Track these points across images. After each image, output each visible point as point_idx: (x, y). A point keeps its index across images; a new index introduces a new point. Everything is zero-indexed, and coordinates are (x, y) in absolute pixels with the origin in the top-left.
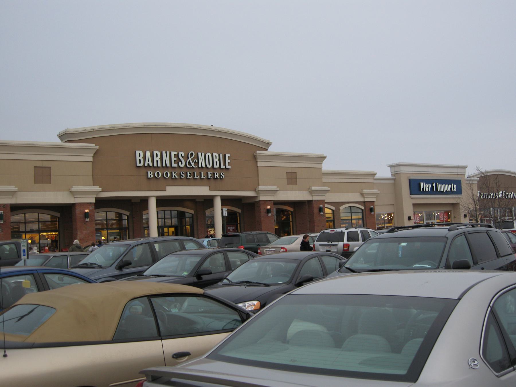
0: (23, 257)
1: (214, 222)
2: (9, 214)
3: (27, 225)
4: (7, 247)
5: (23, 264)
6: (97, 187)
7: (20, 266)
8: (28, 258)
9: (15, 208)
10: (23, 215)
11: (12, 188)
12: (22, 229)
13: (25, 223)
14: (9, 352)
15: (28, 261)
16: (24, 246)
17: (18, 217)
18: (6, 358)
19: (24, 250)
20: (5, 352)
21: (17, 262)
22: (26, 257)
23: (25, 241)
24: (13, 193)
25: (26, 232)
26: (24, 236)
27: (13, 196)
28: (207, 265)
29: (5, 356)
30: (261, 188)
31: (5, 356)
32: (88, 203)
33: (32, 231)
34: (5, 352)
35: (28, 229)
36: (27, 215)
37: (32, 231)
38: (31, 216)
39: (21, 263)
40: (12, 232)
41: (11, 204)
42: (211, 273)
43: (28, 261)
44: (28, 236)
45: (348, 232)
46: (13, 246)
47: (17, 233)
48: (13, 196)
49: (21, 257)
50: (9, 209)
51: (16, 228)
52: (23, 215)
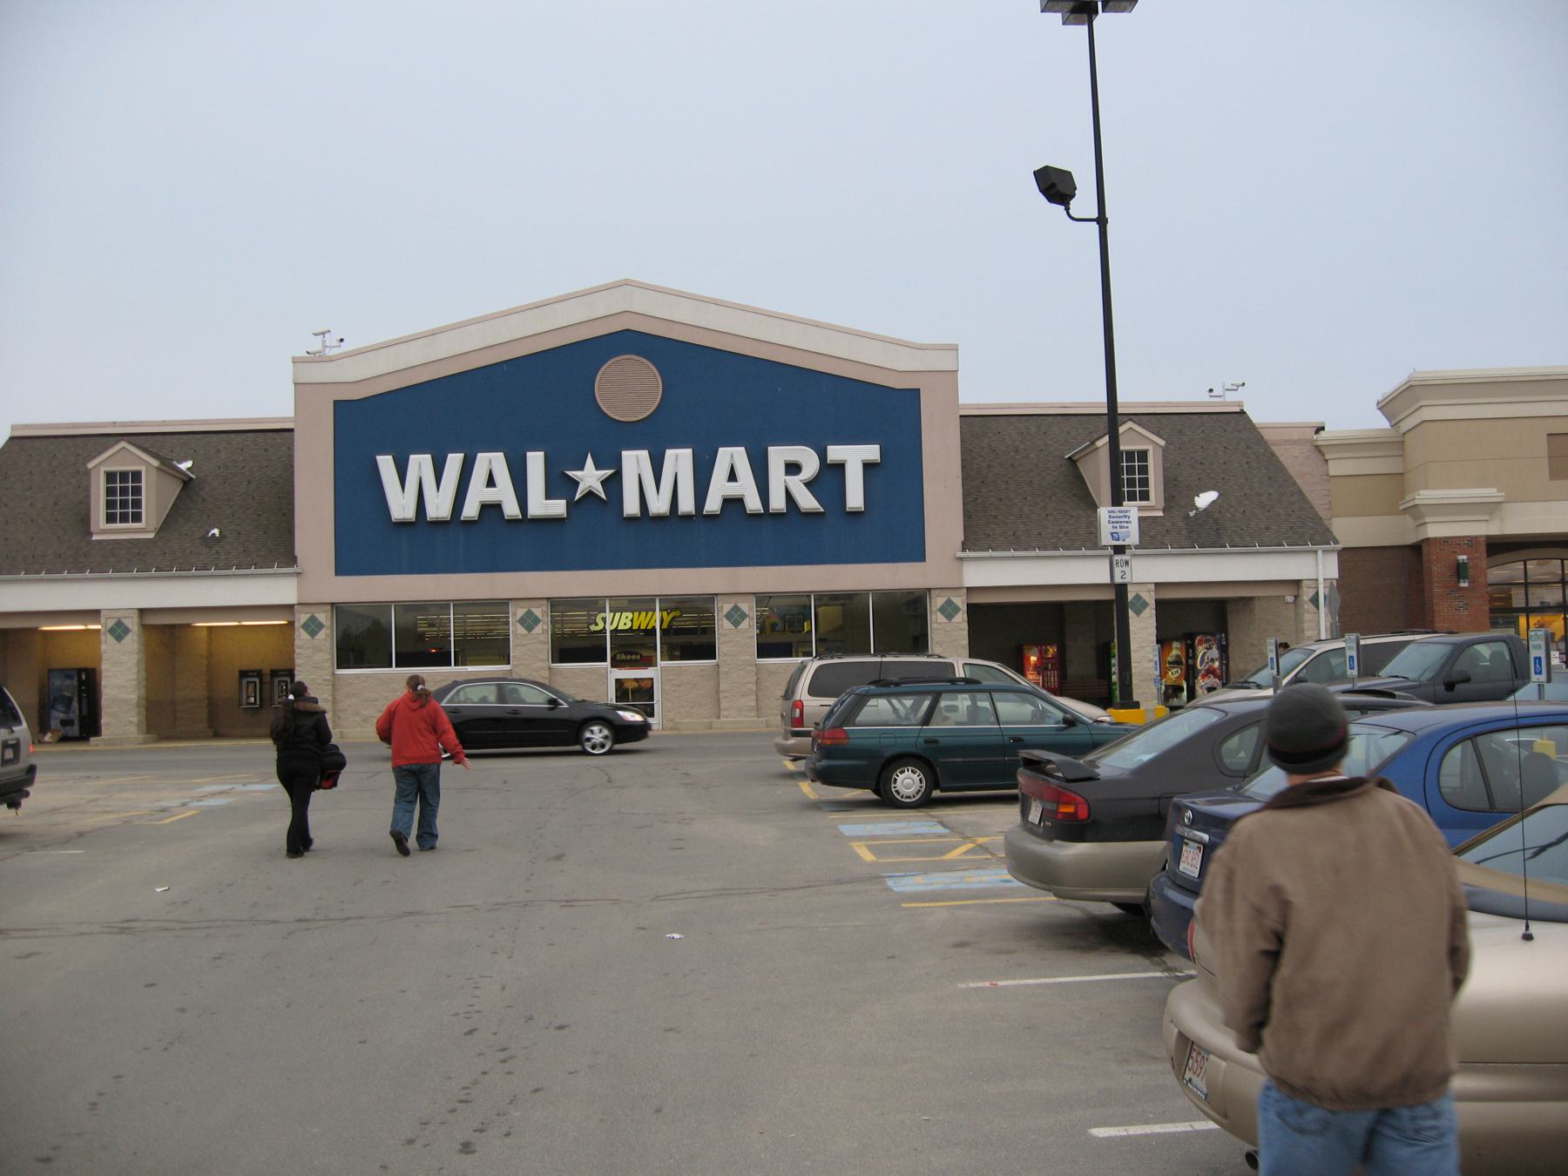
0: (1534, 677)
1: (88, 496)
2: (1484, 562)
3: (1531, 590)
4: (1484, 650)
5: (1535, 696)
6: (1492, 491)
7: (1525, 700)
8: (1549, 680)
9: (1500, 547)
10: (1520, 566)
11: (1490, 493)
12: (1518, 600)
13: (1526, 585)
14: (1536, 928)
15: (1549, 689)
16: (1539, 647)
17: (1507, 571)
18: (1529, 944)
19: (1538, 659)
20: (1527, 927)
21: (1513, 691)
22: (1543, 678)
23: (1535, 635)
24: (1491, 508)
25: (1528, 611)
26: (1522, 621)
27: (1491, 514)
28: (1462, 666)
29: (1528, 937)
30: (1425, 496)
31: (1528, 937)
32: (967, 516)
33: (1543, 609)
34: (1527, 927)
35: (1534, 603)
36: (1531, 566)
37: (1543, 609)
38: (1543, 568)
39: (1527, 692)
40: (1492, 610)
41: (1488, 537)
42: (1467, 680)
43: (1549, 689)
44: (1534, 620)
45: (916, 553)
46: (1503, 647)
47: (1503, 612)
48: (1491, 514)
49: (1528, 677)
50: (1483, 548)
51: (1500, 599)
52: (1520, 566)
